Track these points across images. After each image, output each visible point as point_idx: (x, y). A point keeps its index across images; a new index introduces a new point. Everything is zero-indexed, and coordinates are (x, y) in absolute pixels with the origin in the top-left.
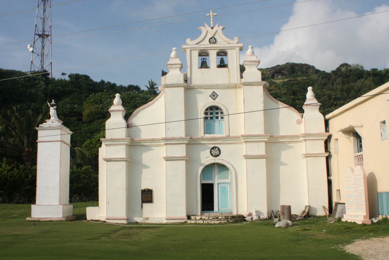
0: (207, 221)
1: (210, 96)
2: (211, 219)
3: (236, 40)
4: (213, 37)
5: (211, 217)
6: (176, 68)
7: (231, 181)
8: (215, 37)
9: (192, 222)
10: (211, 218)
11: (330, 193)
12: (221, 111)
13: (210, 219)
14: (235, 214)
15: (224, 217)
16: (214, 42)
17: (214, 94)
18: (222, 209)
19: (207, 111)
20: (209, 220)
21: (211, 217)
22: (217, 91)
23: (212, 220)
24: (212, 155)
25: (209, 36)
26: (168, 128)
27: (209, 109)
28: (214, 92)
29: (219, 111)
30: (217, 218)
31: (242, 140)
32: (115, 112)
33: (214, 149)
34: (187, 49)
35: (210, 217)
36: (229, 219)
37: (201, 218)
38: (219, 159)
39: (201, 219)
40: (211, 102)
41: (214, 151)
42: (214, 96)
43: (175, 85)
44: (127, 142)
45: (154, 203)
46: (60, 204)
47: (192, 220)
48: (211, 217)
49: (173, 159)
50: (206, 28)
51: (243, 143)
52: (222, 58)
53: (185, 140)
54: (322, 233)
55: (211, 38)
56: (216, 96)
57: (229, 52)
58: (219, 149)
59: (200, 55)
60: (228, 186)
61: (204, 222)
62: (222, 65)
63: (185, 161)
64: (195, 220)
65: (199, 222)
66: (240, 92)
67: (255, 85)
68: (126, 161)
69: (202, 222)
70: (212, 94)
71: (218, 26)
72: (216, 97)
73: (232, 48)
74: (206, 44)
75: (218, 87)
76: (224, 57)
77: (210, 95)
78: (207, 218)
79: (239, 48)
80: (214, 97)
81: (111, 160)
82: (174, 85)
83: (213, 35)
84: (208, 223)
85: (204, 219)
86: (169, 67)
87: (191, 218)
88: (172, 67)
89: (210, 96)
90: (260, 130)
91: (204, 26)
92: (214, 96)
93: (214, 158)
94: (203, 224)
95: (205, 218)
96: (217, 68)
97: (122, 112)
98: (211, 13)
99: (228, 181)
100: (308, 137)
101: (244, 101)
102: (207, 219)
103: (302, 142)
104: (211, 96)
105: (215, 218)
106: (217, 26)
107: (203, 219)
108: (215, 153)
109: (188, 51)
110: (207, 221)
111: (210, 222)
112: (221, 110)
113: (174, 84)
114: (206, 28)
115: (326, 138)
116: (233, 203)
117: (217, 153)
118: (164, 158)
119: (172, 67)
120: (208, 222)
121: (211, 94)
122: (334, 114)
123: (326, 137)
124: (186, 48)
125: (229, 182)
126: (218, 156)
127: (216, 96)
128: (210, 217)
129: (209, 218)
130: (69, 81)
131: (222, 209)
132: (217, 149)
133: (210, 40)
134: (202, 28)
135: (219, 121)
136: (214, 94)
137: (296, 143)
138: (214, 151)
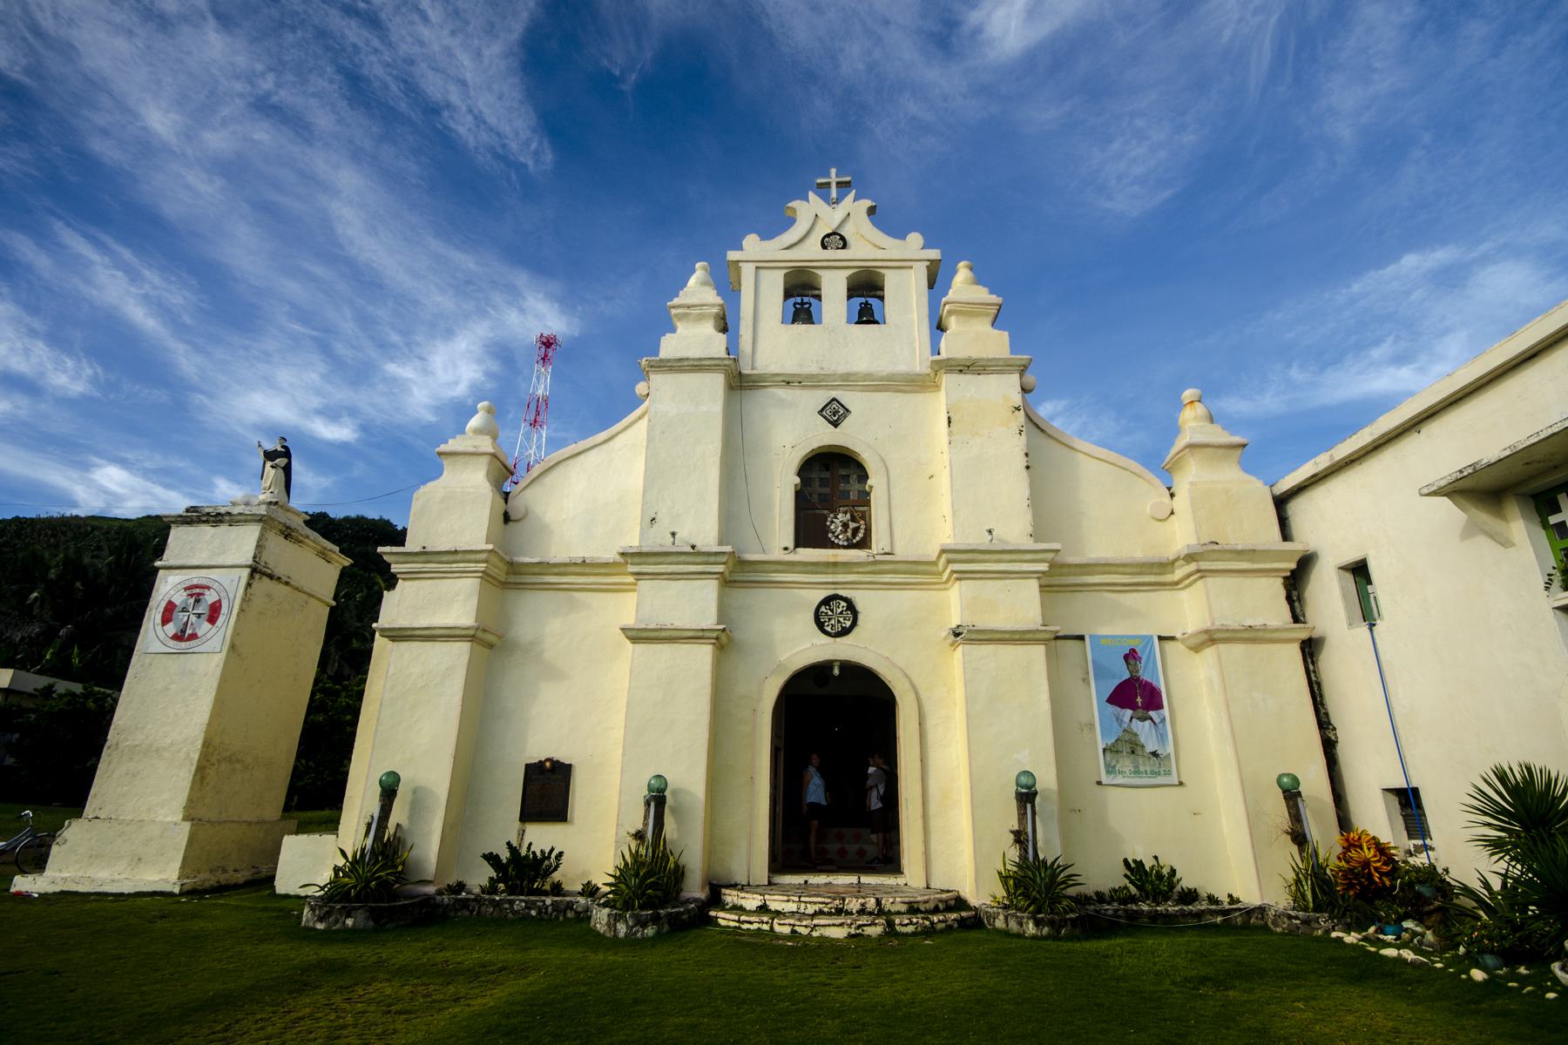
3: (915, 239)
4: (834, 233)
6: (701, 318)
8: (842, 233)
11: (1341, 814)
22: (847, 398)
26: (654, 516)
31: (940, 574)
32: (460, 457)
34: (740, 264)
39: (763, 909)
40: (825, 436)
42: (835, 414)
44: (485, 565)
45: (572, 823)
46: (185, 819)
49: (663, 634)
51: (947, 586)
52: (867, 303)
53: (712, 559)
55: (828, 236)
57: (891, 281)
58: (851, 606)
59: (788, 294)
62: (866, 316)
63: (710, 647)
66: (937, 405)
68: (472, 638)
73: (903, 265)
74: (811, 251)
75: (849, 380)
76: (871, 301)
79: (928, 263)
80: (828, 412)
81: (409, 633)
82: (686, 363)
86: (678, 314)
88: (686, 315)
90: (1015, 529)
91: (807, 200)
92: (835, 414)
93: (832, 639)
97: (485, 460)
98: (833, 171)
100: (1214, 561)
103: (1179, 586)
109: (747, 272)
113: (687, 359)
115: (1293, 566)
119: (686, 315)
122: (1337, 458)
123: (1290, 561)
126: (845, 632)
130: (1513, 892)
134: (795, 204)
137: (1158, 593)
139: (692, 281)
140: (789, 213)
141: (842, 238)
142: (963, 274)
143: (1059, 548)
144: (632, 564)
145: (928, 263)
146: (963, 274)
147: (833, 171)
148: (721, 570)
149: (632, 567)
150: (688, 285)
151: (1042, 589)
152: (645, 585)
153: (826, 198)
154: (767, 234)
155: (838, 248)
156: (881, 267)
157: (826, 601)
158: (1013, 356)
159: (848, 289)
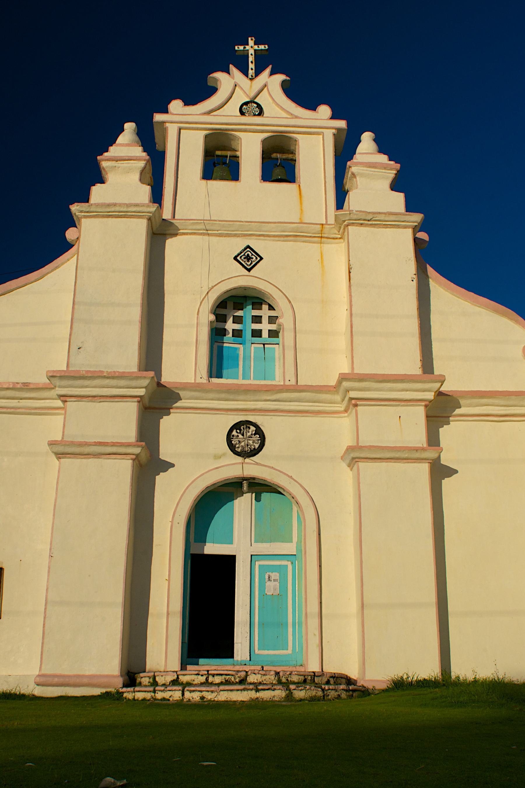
0: (201, 691)
1: (235, 258)
2: (218, 685)
3: (325, 111)
5: (217, 675)
7: (298, 549)
9: (140, 696)
10: (217, 680)
12: (272, 313)
13: (212, 684)
14: (313, 667)
15: (273, 677)
16: (257, 113)
17: (250, 255)
18: (266, 652)
19: (222, 311)
20: (208, 689)
21: (217, 675)
22: (257, 245)
23: (222, 687)
24: (232, 447)
25: (240, 98)
27: (230, 305)
28: (248, 247)
29: (265, 312)
30: (242, 681)
33: (240, 430)
35: (213, 675)
36: (292, 687)
37: (178, 678)
38: (257, 464)
41: (243, 435)
43: (117, 209)
47: (137, 689)
48: (216, 677)
50: (233, 78)
54: (123, 702)
55: (246, 104)
56: (256, 258)
58: (259, 432)
60: (290, 567)
61: (187, 695)
64: (152, 689)
65: (167, 695)
67: (386, 226)
69: (177, 695)
70: (241, 253)
71: (272, 73)
72: (254, 263)
77: (236, 254)
78: (203, 679)
79: (334, 131)
80: (249, 263)
83: (252, 95)
84: (202, 698)
85: (189, 684)
87: (138, 680)
89: (235, 258)
91: (228, 72)
93: (240, 459)
94: (180, 704)
95: (193, 677)
96: (260, 182)
98: (251, 42)
99: (289, 548)
101: (350, 272)
102: (202, 684)
104: (238, 258)
105: (233, 679)
106: (268, 71)
107: (182, 684)
108: (243, 444)
109: (172, 131)
110: (201, 691)
111: (209, 696)
112: (271, 308)
113: (115, 205)
114: (233, 78)
116: (306, 592)
117: (251, 442)
118: (52, 444)
120: (205, 694)
121: (238, 252)
124: (165, 122)
125: (298, 384)
126: (254, 452)
127: (254, 258)
128: (213, 675)
129: (207, 679)
131: (266, 652)
132: (253, 428)
133: (245, 107)
134: (219, 75)
135: (264, 344)
136: (249, 253)
138: (240, 436)
139: (121, 139)
140: (210, 83)
141: (259, 106)
142: (367, 139)
143: (242, 315)
144: (60, 387)
145: (334, 131)
146: (367, 139)
147: (251, 42)
148: (142, 394)
149: (60, 389)
150: (117, 142)
151: (429, 419)
152: (71, 405)
153: (245, 72)
154: (190, 101)
155: (255, 115)
156: (294, 132)
157: (237, 426)
158: (295, 539)
159: (263, 152)
